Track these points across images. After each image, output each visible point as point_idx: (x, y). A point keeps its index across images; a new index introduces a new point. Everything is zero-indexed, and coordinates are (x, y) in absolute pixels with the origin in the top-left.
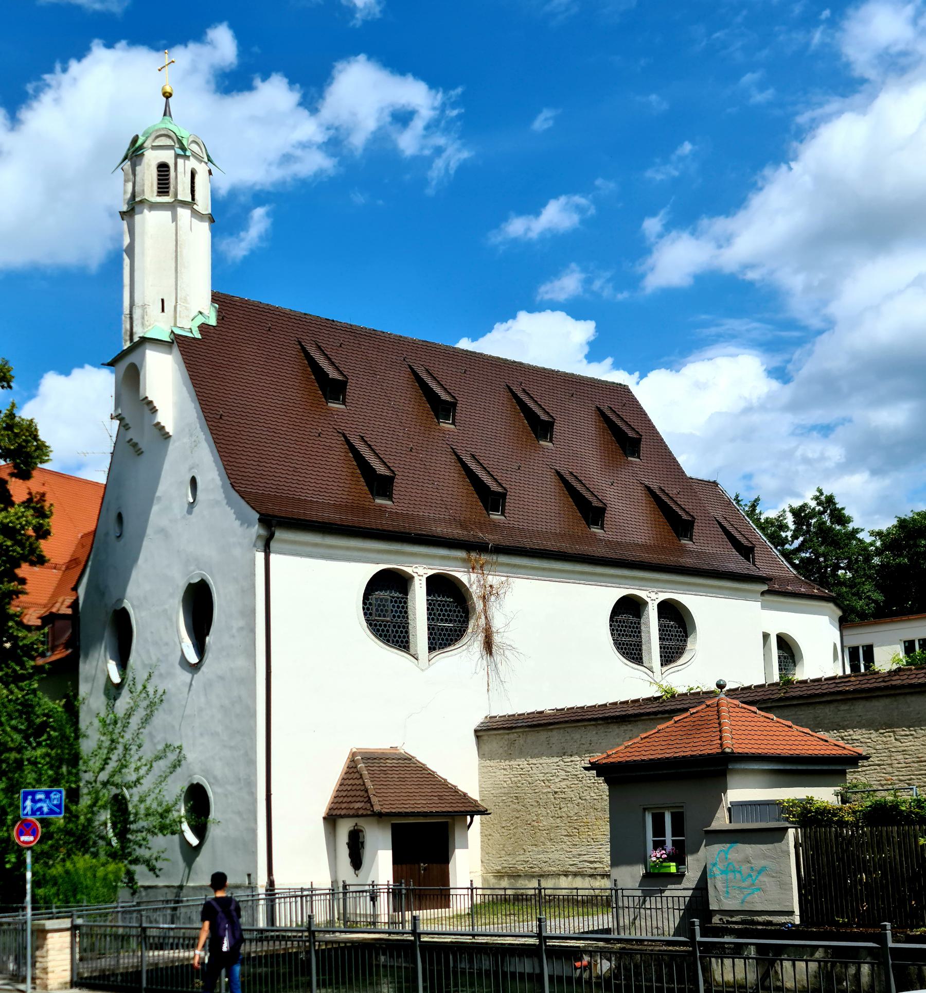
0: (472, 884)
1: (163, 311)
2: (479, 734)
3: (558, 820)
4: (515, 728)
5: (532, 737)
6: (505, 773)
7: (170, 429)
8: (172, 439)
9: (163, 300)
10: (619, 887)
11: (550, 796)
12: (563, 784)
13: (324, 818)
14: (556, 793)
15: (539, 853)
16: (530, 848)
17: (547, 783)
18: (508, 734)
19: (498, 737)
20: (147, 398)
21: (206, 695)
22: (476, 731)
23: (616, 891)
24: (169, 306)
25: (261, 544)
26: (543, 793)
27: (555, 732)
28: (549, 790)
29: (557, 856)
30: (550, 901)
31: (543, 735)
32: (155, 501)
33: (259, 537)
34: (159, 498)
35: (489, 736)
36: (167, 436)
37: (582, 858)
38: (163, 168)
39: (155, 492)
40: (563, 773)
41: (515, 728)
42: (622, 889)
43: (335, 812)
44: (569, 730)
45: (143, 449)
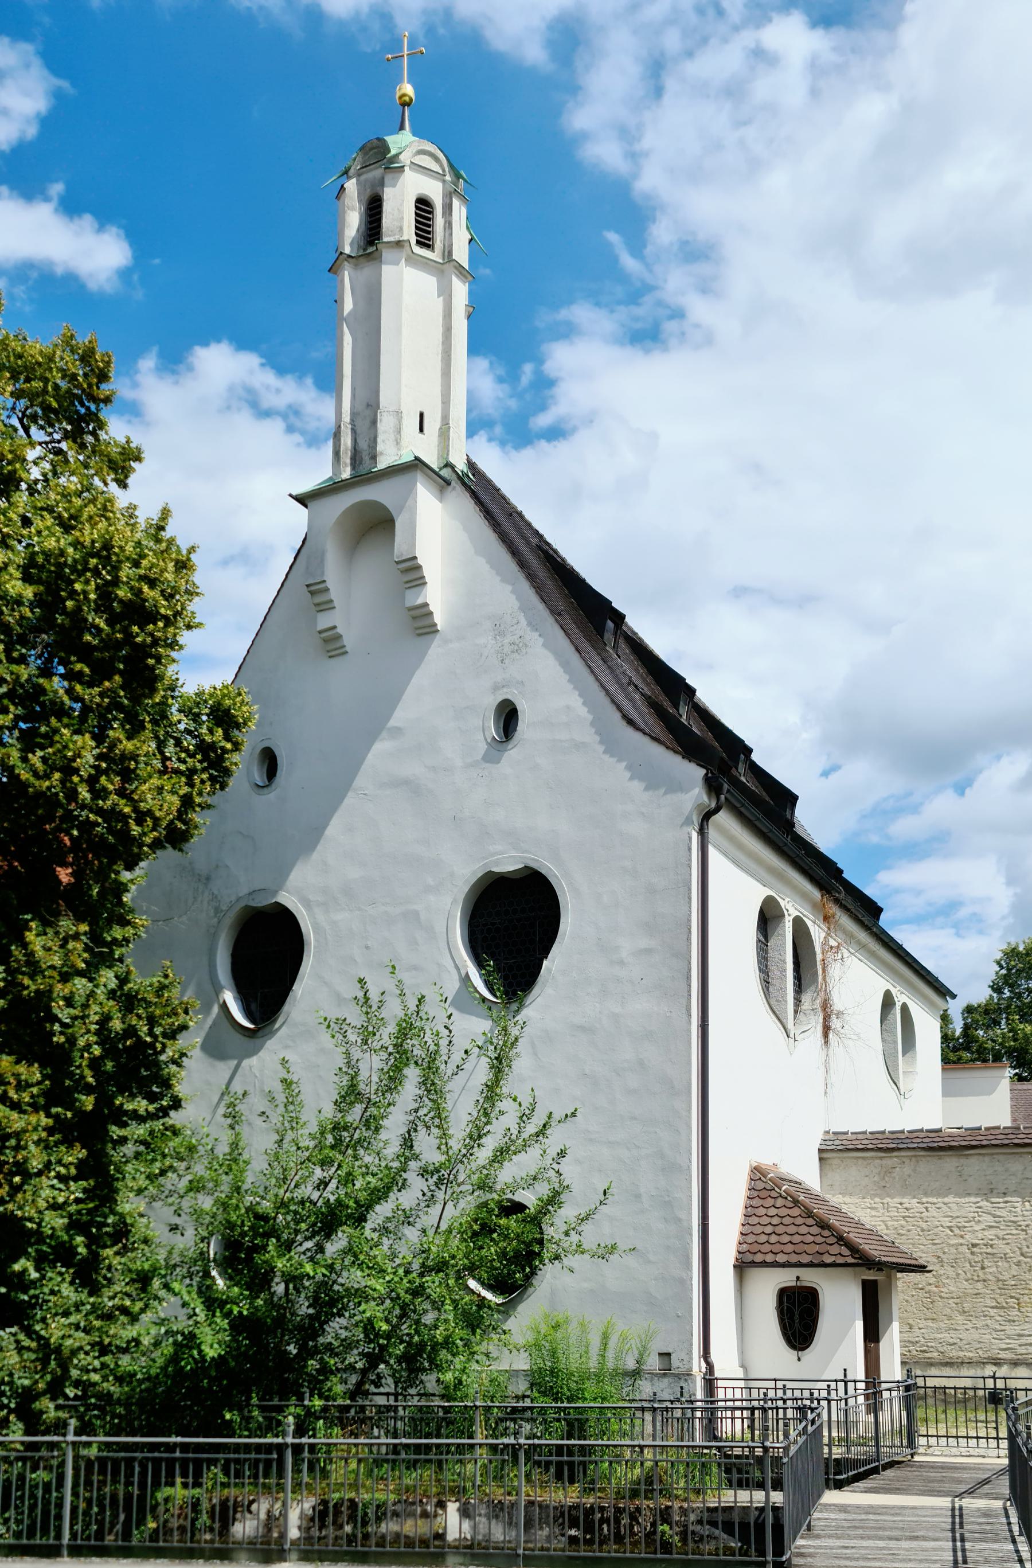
0: (845, 1376)
1: (421, 430)
2: (825, 1155)
3: (979, 1285)
4: (899, 1149)
5: (928, 1165)
6: (874, 1213)
7: (438, 619)
8: (438, 639)
9: (422, 415)
10: (849, 1378)
11: (964, 1249)
12: (990, 1234)
13: (735, 1266)
14: (974, 1245)
15: (939, 1330)
16: (922, 1324)
17: (957, 1231)
18: (881, 1158)
19: (860, 1161)
20: (415, 558)
21: (535, 1054)
22: (820, 1151)
23: (846, 1383)
24: (432, 424)
25: (696, 820)
26: (949, 1245)
27: (973, 1160)
28: (961, 1241)
29: (976, 1336)
30: (965, 1401)
31: (950, 1163)
32: (384, 734)
33: (699, 806)
34: (397, 732)
35: (842, 1159)
36: (431, 630)
37: (1024, 1340)
38: (423, 205)
39: (389, 718)
40: (990, 1218)
41: (899, 1149)
42: (855, 1381)
43: (749, 1258)
44: (1001, 1157)
45: (347, 649)
